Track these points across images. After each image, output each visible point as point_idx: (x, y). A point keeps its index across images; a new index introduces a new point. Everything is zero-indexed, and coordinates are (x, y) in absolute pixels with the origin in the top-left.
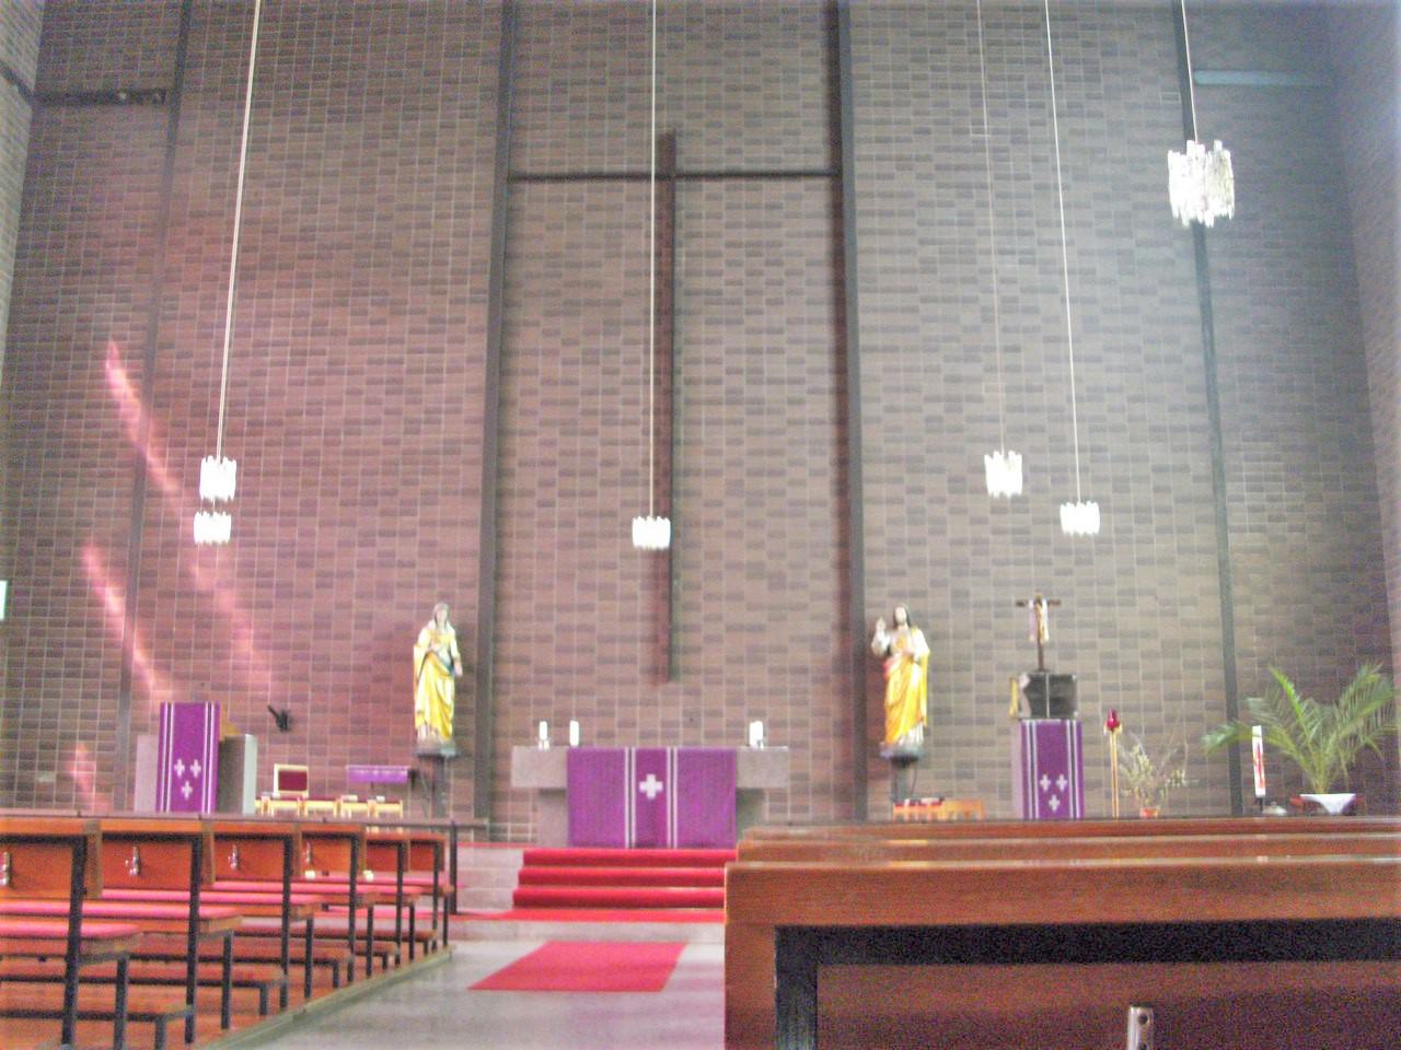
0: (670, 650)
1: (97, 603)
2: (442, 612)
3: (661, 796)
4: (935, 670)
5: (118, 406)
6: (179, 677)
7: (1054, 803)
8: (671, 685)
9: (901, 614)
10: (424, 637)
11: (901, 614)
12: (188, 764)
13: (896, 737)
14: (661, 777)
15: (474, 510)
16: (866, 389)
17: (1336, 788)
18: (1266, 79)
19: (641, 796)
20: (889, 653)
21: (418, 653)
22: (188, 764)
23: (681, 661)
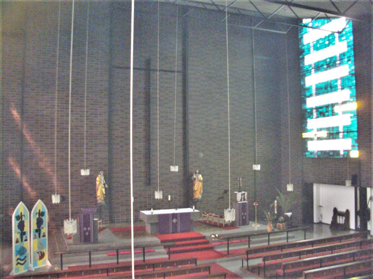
0: (149, 179)
1: (12, 171)
2: (102, 173)
3: (177, 222)
4: (204, 182)
5: (14, 120)
6: (37, 189)
7: (244, 218)
8: (149, 187)
9: (197, 171)
10: (98, 179)
11: (197, 171)
12: (87, 228)
13: (197, 197)
14: (176, 219)
15: (106, 148)
16: (190, 122)
17: (288, 212)
18: (265, 58)
19: (173, 222)
20: (195, 180)
21: (98, 183)
22: (87, 228)
23: (152, 181)
